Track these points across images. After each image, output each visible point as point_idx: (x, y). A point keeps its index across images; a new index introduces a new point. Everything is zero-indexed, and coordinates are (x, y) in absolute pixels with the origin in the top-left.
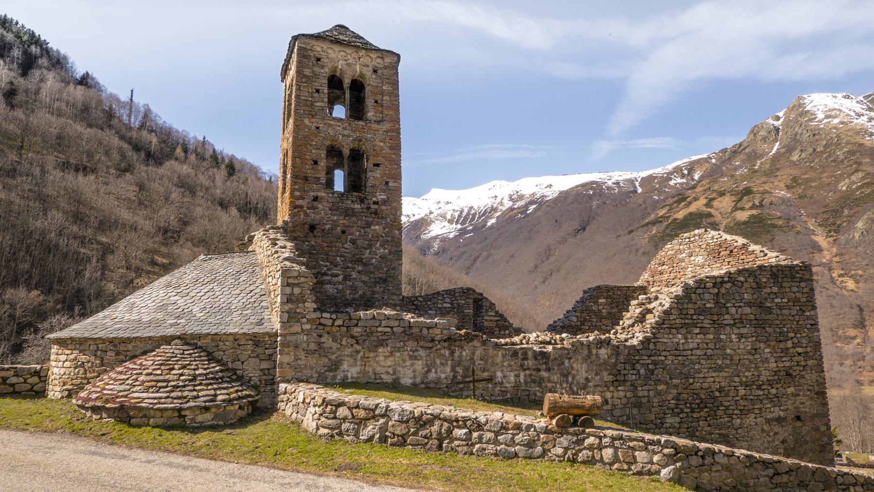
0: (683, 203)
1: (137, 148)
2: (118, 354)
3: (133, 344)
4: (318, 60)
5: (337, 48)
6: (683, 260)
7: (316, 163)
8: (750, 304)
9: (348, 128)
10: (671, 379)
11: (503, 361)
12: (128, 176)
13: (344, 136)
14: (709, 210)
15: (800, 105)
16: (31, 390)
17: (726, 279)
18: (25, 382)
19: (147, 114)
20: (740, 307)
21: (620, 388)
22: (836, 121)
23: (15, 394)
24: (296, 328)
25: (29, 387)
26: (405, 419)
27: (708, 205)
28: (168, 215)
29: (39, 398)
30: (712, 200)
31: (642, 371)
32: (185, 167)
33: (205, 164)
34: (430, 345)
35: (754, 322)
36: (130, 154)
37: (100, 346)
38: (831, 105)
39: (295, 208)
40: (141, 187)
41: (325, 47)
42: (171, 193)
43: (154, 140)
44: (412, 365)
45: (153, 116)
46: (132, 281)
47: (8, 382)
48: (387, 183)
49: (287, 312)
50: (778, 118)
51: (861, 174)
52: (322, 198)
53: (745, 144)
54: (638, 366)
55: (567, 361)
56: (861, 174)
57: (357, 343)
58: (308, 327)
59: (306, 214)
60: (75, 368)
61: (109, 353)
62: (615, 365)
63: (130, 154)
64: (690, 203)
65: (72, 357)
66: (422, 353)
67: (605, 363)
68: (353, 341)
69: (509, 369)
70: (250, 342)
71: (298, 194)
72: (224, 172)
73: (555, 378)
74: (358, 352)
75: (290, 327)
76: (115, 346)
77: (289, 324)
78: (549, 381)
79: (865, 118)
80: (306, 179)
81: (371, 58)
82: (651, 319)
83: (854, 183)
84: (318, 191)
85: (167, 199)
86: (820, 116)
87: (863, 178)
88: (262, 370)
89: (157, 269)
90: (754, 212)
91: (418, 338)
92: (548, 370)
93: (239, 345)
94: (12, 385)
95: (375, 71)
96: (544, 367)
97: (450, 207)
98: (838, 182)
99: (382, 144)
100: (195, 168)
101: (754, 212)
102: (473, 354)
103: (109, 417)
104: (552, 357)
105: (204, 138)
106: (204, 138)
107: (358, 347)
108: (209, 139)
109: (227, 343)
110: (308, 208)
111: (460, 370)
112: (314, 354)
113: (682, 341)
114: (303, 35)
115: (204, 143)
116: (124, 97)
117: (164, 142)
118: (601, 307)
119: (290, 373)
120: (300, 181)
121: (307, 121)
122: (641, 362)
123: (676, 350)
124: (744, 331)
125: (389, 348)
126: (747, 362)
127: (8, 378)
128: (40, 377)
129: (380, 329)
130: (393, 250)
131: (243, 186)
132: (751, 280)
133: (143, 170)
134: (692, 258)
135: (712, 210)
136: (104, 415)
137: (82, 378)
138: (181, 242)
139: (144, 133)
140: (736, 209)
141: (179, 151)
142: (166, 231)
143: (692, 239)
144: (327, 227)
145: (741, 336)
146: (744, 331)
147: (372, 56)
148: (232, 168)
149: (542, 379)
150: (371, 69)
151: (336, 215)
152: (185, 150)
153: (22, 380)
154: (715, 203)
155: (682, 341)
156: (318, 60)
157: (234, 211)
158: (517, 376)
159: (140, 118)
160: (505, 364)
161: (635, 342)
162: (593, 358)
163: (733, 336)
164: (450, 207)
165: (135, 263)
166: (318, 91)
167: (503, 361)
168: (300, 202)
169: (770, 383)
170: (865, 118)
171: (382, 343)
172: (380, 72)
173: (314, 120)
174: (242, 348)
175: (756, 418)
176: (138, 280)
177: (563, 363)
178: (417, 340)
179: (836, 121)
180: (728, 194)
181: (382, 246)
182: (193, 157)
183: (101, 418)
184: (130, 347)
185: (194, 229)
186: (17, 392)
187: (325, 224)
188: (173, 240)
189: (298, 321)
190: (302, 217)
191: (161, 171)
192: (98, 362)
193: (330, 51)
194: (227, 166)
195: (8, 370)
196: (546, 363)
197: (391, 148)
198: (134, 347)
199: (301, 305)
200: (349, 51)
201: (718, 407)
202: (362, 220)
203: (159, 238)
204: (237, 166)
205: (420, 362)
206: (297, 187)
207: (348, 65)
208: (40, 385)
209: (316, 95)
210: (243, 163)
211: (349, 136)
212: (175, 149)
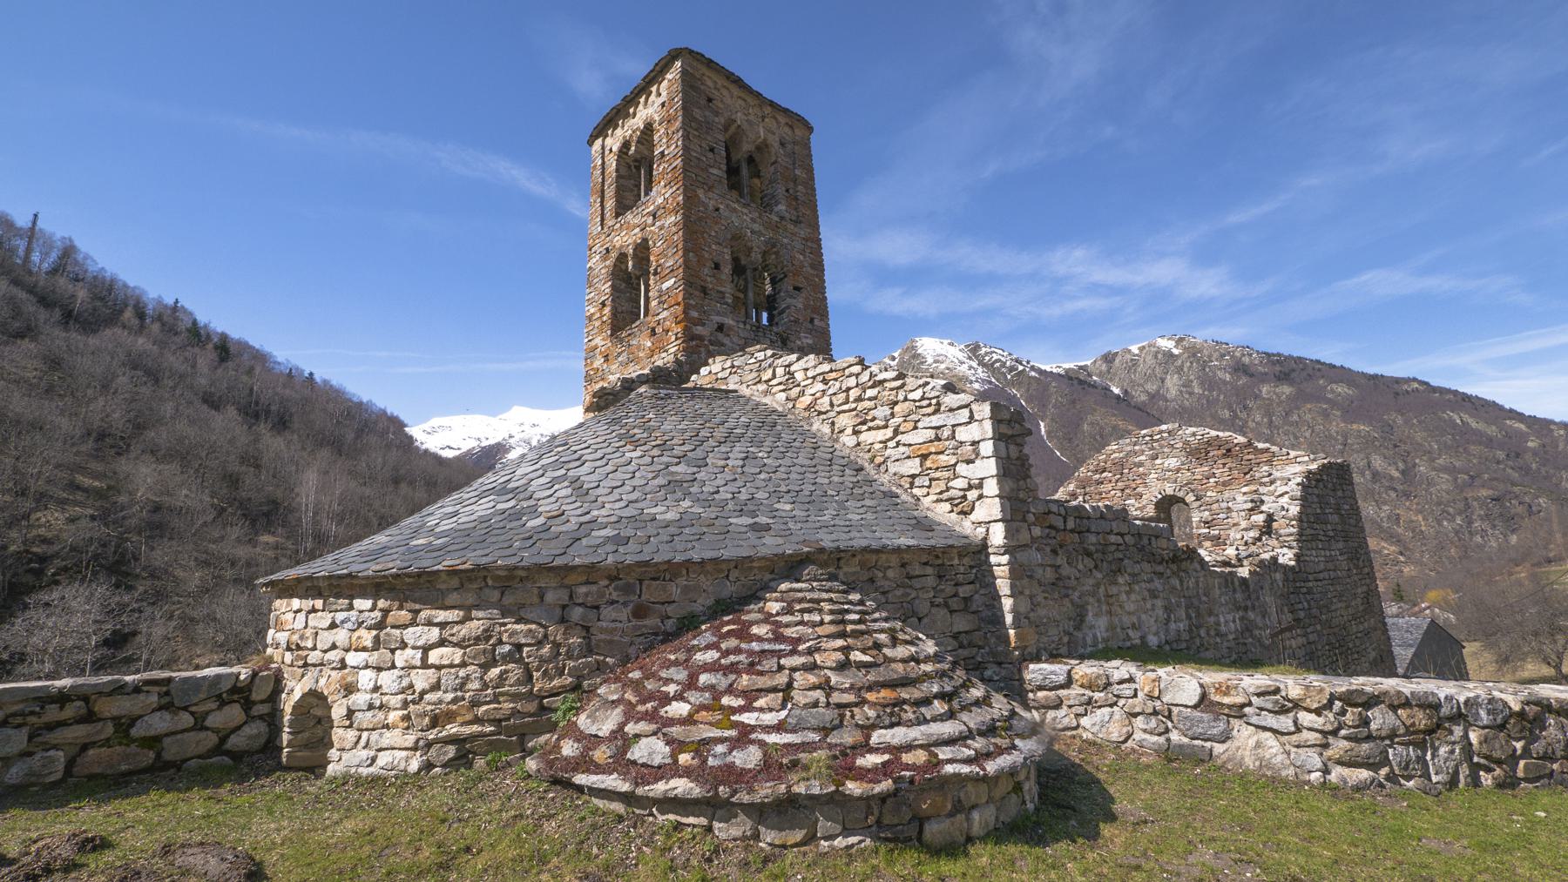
1: (45, 301)
2: (640, 612)
3: (682, 581)
4: (710, 100)
6: (1140, 464)
7: (717, 266)
12: (26, 344)
15: (914, 348)
16: (218, 749)
18: (199, 725)
19: (68, 251)
22: (942, 366)
23: (163, 770)
25: (213, 739)
26: (1499, 721)
28: (111, 411)
29: (242, 779)
32: (141, 341)
33: (178, 339)
36: (32, 309)
37: (583, 589)
38: (939, 351)
39: (692, 339)
40: (54, 363)
42: (115, 376)
43: (82, 294)
45: (80, 257)
46: (26, 517)
47: (134, 732)
48: (812, 320)
50: (893, 359)
52: (730, 328)
60: (485, 667)
61: (607, 612)
63: (32, 309)
65: (475, 627)
70: (929, 570)
72: (213, 356)
74: (1097, 585)
76: (627, 589)
79: (965, 366)
80: (704, 290)
84: (725, 315)
85: (105, 387)
86: (930, 360)
88: (956, 636)
89: (80, 496)
94: (153, 742)
97: (538, 430)
100: (162, 344)
103: (846, 832)
105: (177, 301)
106: (177, 301)
108: (184, 302)
114: (691, 52)
115: (175, 308)
116: (22, 221)
117: (102, 299)
127: (133, 721)
128: (248, 705)
131: (245, 378)
133: (58, 338)
134: (1158, 461)
136: (824, 825)
137: (515, 697)
138: (132, 455)
139: (62, 281)
141: (128, 314)
142: (102, 436)
148: (225, 349)
152: (141, 315)
153: (186, 720)
156: (710, 100)
157: (232, 412)
159: (54, 256)
164: (538, 430)
165: (35, 486)
166: (712, 150)
168: (699, 330)
170: (965, 366)
172: (789, 147)
173: (711, 195)
174: (916, 583)
176: (39, 514)
179: (942, 366)
182: (156, 327)
183: (811, 839)
184: (675, 590)
185: (160, 436)
186: (168, 765)
188: (113, 451)
189: (1024, 520)
191: (93, 341)
192: (575, 640)
193: (725, 92)
194: (216, 347)
195: (137, 689)
197: (812, 266)
198: (686, 590)
203: (91, 444)
204: (232, 350)
208: (249, 730)
209: (710, 155)
210: (244, 346)
211: (760, 234)
212: (121, 312)
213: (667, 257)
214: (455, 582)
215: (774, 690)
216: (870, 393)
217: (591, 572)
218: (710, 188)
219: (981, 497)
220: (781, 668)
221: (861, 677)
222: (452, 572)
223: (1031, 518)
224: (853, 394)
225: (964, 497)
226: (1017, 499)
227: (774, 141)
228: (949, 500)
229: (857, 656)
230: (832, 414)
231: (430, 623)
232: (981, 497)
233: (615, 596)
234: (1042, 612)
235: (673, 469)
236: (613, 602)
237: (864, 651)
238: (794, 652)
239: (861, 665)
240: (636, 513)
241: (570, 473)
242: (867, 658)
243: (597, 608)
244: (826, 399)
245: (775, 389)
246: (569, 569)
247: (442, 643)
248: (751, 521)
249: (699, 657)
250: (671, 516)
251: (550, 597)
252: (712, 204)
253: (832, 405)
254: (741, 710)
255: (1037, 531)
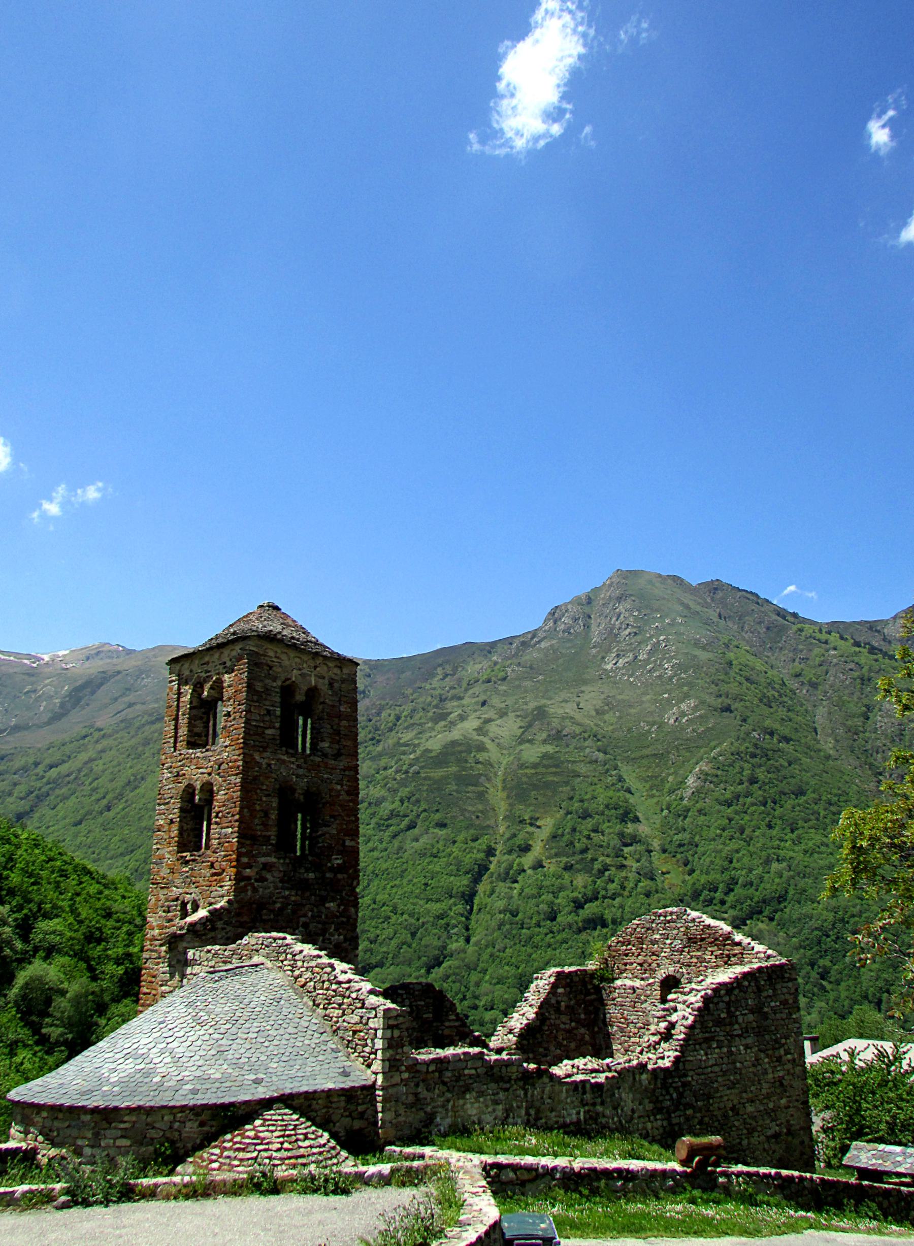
0: (443, 723)
5: (292, 654)
6: (654, 942)
8: (752, 1012)
9: (303, 765)
10: (696, 1101)
11: (567, 1098)
13: (297, 776)
14: (481, 738)
17: (735, 985)
20: (745, 1014)
21: (658, 1117)
24: (396, 1079)
27: (480, 730)
30: (488, 721)
31: (675, 1095)
34: (508, 1085)
35: (757, 1030)
37: (180, 1115)
41: (279, 651)
44: (494, 1110)
49: (388, 1060)
51: (692, 702)
53: (541, 635)
54: (671, 1090)
55: (616, 1091)
56: (692, 702)
57: (448, 1090)
58: (406, 1075)
59: (255, 890)
61: (189, 1124)
62: (654, 1090)
64: (453, 724)
66: (502, 1095)
67: (646, 1090)
68: (445, 1088)
69: (572, 1105)
71: (245, 860)
73: (608, 1112)
74: (448, 1101)
75: (392, 1077)
76: (197, 1115)
77: (390, 1074)
78: (604, 1116)
81: (329, 667)
82: (679, 1033)
83: (683, 714)
87: (695, 709)
90: (550, 749)
91: (499, 1079)
92: (602, 1103)
93: (331, 1102)
95: (331, 685)
96: (599, 1100)
98: (663, 710)
99: (339, 787)
101: (550, 749)
102: (543, 1092)
104: (605, 1088)
107: (449, 1095)
109: (320, 1101)
110: (257, 880)
111: (532, 1112)
112: (412, 1107)
113: (704, 1058)
118: (559, 998)
119: (392, 1133)
120: (248, 842)
121: (257, 757)
122: (674, 1085)
123: (700, 1068)
124: (749, 1041)
125: (474, 1094)
126: (752, 1075)
129: (466, 1072)
130: (349, 936)
132: (753, 984)
135: (486, 740)
140: (521, 740)
143: (669, 918)
144: (278, 905)
145: (747, 1047)
146: (749, 1041)
147: (330, 665)
149: (597, 1114)
150: (326, 682)
151: (288, 889)
154: (493, 728)
155: (704, 1058)
158: (578, 1113)
160: (569, 1100)
161: (666, 1063)
162: (637, 1085)
163: (742, 1048)
167: (567, 1098)
169: (768, 1096)
171: (467, 1089)
175: (759, 1136)
177: (614, 1094)
178: (497, 1082)
180: (511, 715)
181: (336, 930)
187: (275, 902)
189: (398, 1070)
190: (249, 893)
193: (284, 657)
196: (601, 1096)
197: (348, 793)
199: (400, 1050)
200: (305, 658)
201: (730, 1128)
202: (315, 895)
205: (500, 1107)
206: (244, 850)
207: (303, 675)
213: (226, 795)
214: (128, 1111)
215: (251, 1158)
216: (334, 987)
217: (183, 1108)
218: (265, 749)
219: (376, 1058)
220: (255, 1150)
221: (285, 1154)
222: (128, 1108)
223: (403, 1068)
224: (326, 985)
225: (369, 1057)
226: (395, 1060)
227: (323, 686)
228: (362, 1057)
229: (286, 1145)
230: (314, 994)
231: (115, 1128)
232: (376, 1058)
233: (192, 1117)
234: (401, 1119)
235: (220, 1042)
236: (190, 1120)
237: (290, 1143)
238: (261, 1144)
239: (287, 1150)
240: (201, 1074)
241: (169, 1046)
242: (290, 1147)
243: (184, 1122)
244: (312, 983)
245: (286, 968)
246: (174, 1107)
247: (122, 1137)
248: (254, 1077)
249: (225, 1144)
250: (218, 1075)
251: (166, 1118)
252: (264, 762)
253: (315, 988)
254: (238, 1166)
255: (406, 1075)
